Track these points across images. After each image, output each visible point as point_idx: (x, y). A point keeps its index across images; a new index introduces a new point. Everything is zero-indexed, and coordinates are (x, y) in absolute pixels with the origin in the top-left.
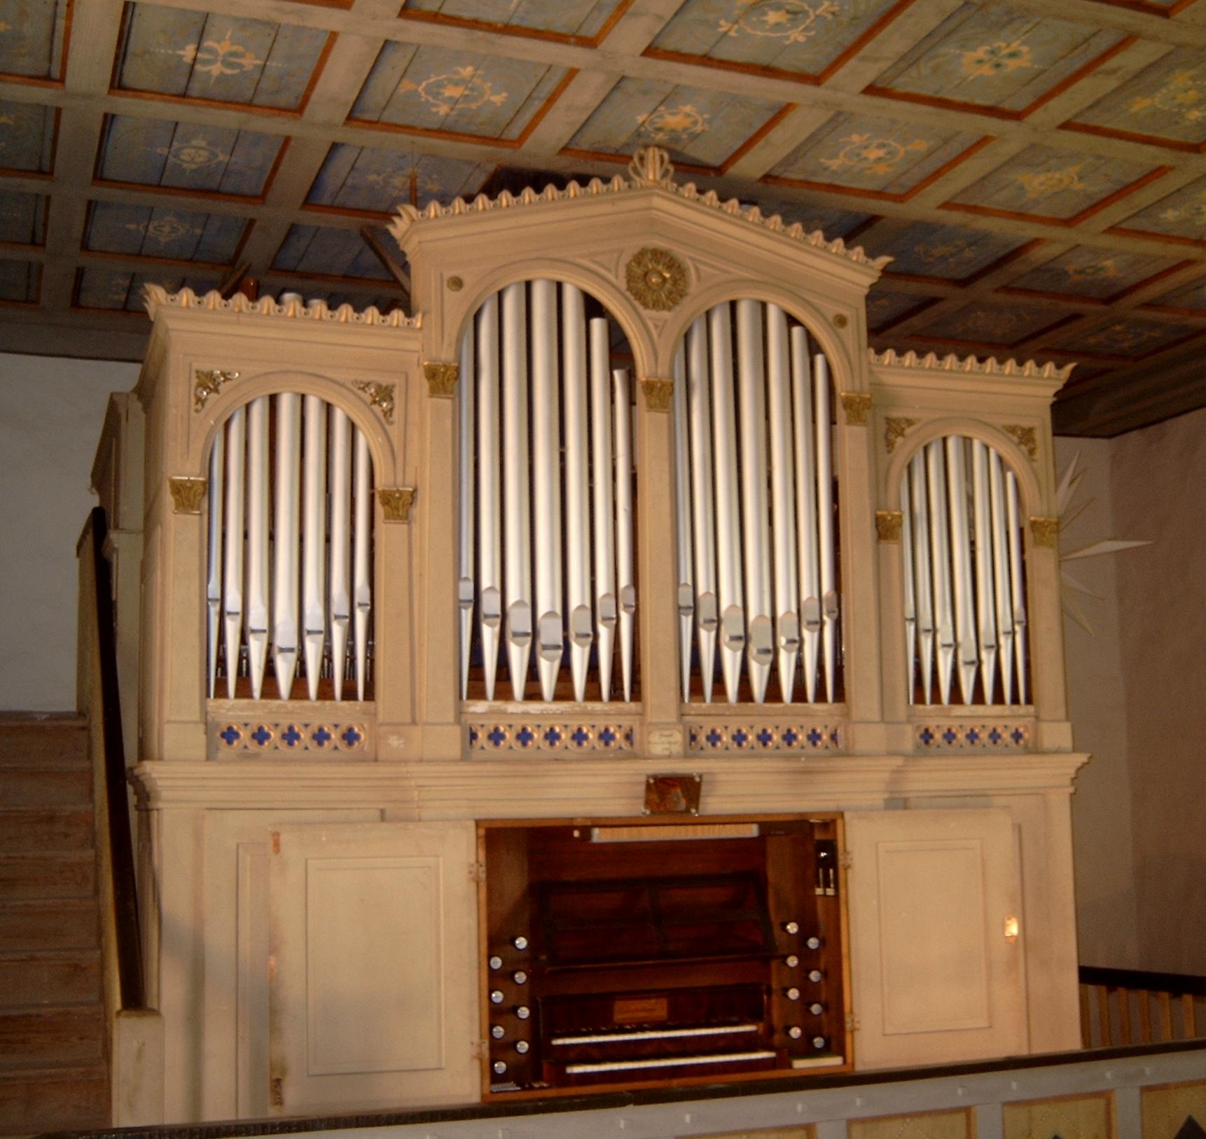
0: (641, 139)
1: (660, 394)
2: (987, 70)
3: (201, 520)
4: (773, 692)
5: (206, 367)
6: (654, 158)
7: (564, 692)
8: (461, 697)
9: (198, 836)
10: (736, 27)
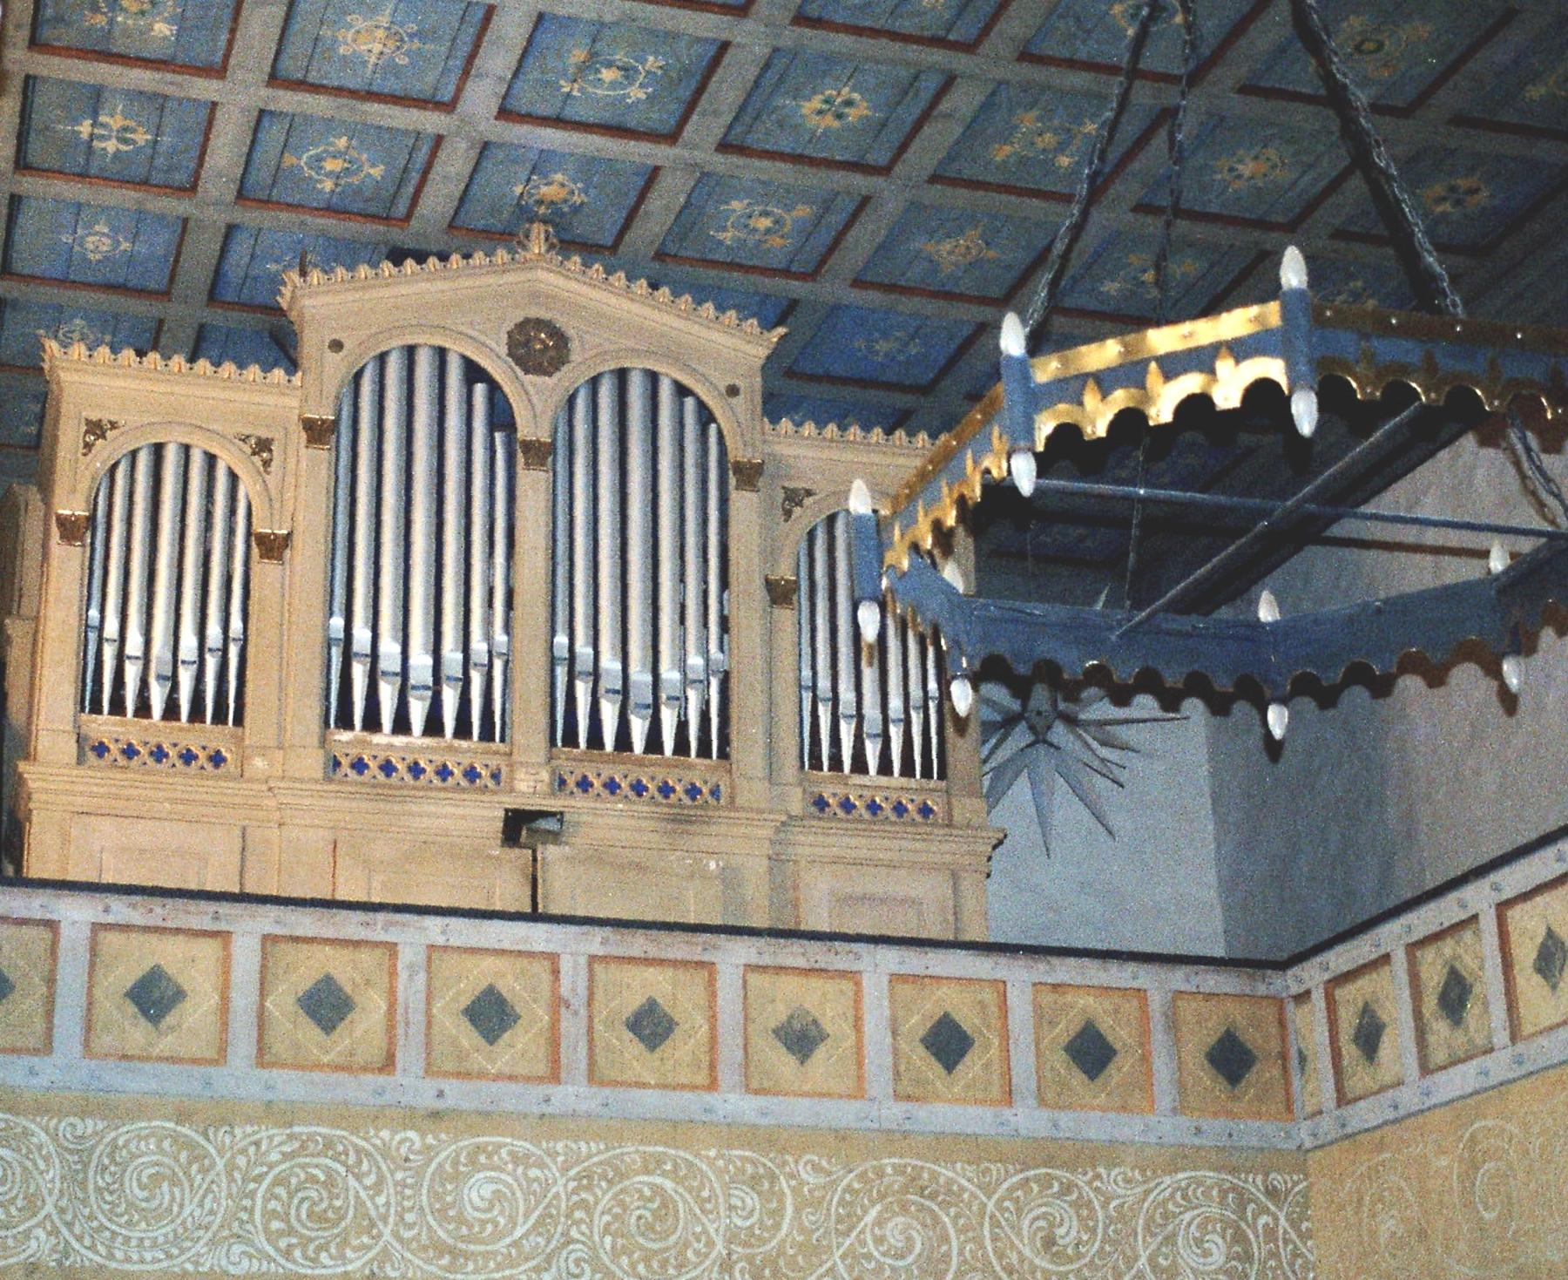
0: (525, 213)
1: (539, 453)
2: (829, 121)
3: (84, 552)
4: (654, 742)
5: (94, 417)
6: (539, 233)
7: (433, 725)
8: (327, 724)
9: (66, 839)
10: (576, 86)
